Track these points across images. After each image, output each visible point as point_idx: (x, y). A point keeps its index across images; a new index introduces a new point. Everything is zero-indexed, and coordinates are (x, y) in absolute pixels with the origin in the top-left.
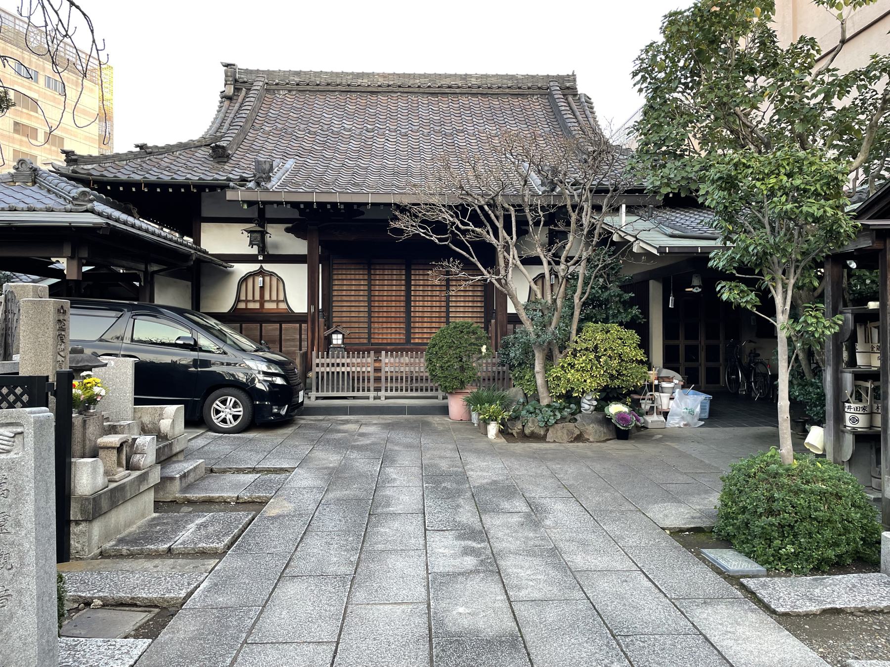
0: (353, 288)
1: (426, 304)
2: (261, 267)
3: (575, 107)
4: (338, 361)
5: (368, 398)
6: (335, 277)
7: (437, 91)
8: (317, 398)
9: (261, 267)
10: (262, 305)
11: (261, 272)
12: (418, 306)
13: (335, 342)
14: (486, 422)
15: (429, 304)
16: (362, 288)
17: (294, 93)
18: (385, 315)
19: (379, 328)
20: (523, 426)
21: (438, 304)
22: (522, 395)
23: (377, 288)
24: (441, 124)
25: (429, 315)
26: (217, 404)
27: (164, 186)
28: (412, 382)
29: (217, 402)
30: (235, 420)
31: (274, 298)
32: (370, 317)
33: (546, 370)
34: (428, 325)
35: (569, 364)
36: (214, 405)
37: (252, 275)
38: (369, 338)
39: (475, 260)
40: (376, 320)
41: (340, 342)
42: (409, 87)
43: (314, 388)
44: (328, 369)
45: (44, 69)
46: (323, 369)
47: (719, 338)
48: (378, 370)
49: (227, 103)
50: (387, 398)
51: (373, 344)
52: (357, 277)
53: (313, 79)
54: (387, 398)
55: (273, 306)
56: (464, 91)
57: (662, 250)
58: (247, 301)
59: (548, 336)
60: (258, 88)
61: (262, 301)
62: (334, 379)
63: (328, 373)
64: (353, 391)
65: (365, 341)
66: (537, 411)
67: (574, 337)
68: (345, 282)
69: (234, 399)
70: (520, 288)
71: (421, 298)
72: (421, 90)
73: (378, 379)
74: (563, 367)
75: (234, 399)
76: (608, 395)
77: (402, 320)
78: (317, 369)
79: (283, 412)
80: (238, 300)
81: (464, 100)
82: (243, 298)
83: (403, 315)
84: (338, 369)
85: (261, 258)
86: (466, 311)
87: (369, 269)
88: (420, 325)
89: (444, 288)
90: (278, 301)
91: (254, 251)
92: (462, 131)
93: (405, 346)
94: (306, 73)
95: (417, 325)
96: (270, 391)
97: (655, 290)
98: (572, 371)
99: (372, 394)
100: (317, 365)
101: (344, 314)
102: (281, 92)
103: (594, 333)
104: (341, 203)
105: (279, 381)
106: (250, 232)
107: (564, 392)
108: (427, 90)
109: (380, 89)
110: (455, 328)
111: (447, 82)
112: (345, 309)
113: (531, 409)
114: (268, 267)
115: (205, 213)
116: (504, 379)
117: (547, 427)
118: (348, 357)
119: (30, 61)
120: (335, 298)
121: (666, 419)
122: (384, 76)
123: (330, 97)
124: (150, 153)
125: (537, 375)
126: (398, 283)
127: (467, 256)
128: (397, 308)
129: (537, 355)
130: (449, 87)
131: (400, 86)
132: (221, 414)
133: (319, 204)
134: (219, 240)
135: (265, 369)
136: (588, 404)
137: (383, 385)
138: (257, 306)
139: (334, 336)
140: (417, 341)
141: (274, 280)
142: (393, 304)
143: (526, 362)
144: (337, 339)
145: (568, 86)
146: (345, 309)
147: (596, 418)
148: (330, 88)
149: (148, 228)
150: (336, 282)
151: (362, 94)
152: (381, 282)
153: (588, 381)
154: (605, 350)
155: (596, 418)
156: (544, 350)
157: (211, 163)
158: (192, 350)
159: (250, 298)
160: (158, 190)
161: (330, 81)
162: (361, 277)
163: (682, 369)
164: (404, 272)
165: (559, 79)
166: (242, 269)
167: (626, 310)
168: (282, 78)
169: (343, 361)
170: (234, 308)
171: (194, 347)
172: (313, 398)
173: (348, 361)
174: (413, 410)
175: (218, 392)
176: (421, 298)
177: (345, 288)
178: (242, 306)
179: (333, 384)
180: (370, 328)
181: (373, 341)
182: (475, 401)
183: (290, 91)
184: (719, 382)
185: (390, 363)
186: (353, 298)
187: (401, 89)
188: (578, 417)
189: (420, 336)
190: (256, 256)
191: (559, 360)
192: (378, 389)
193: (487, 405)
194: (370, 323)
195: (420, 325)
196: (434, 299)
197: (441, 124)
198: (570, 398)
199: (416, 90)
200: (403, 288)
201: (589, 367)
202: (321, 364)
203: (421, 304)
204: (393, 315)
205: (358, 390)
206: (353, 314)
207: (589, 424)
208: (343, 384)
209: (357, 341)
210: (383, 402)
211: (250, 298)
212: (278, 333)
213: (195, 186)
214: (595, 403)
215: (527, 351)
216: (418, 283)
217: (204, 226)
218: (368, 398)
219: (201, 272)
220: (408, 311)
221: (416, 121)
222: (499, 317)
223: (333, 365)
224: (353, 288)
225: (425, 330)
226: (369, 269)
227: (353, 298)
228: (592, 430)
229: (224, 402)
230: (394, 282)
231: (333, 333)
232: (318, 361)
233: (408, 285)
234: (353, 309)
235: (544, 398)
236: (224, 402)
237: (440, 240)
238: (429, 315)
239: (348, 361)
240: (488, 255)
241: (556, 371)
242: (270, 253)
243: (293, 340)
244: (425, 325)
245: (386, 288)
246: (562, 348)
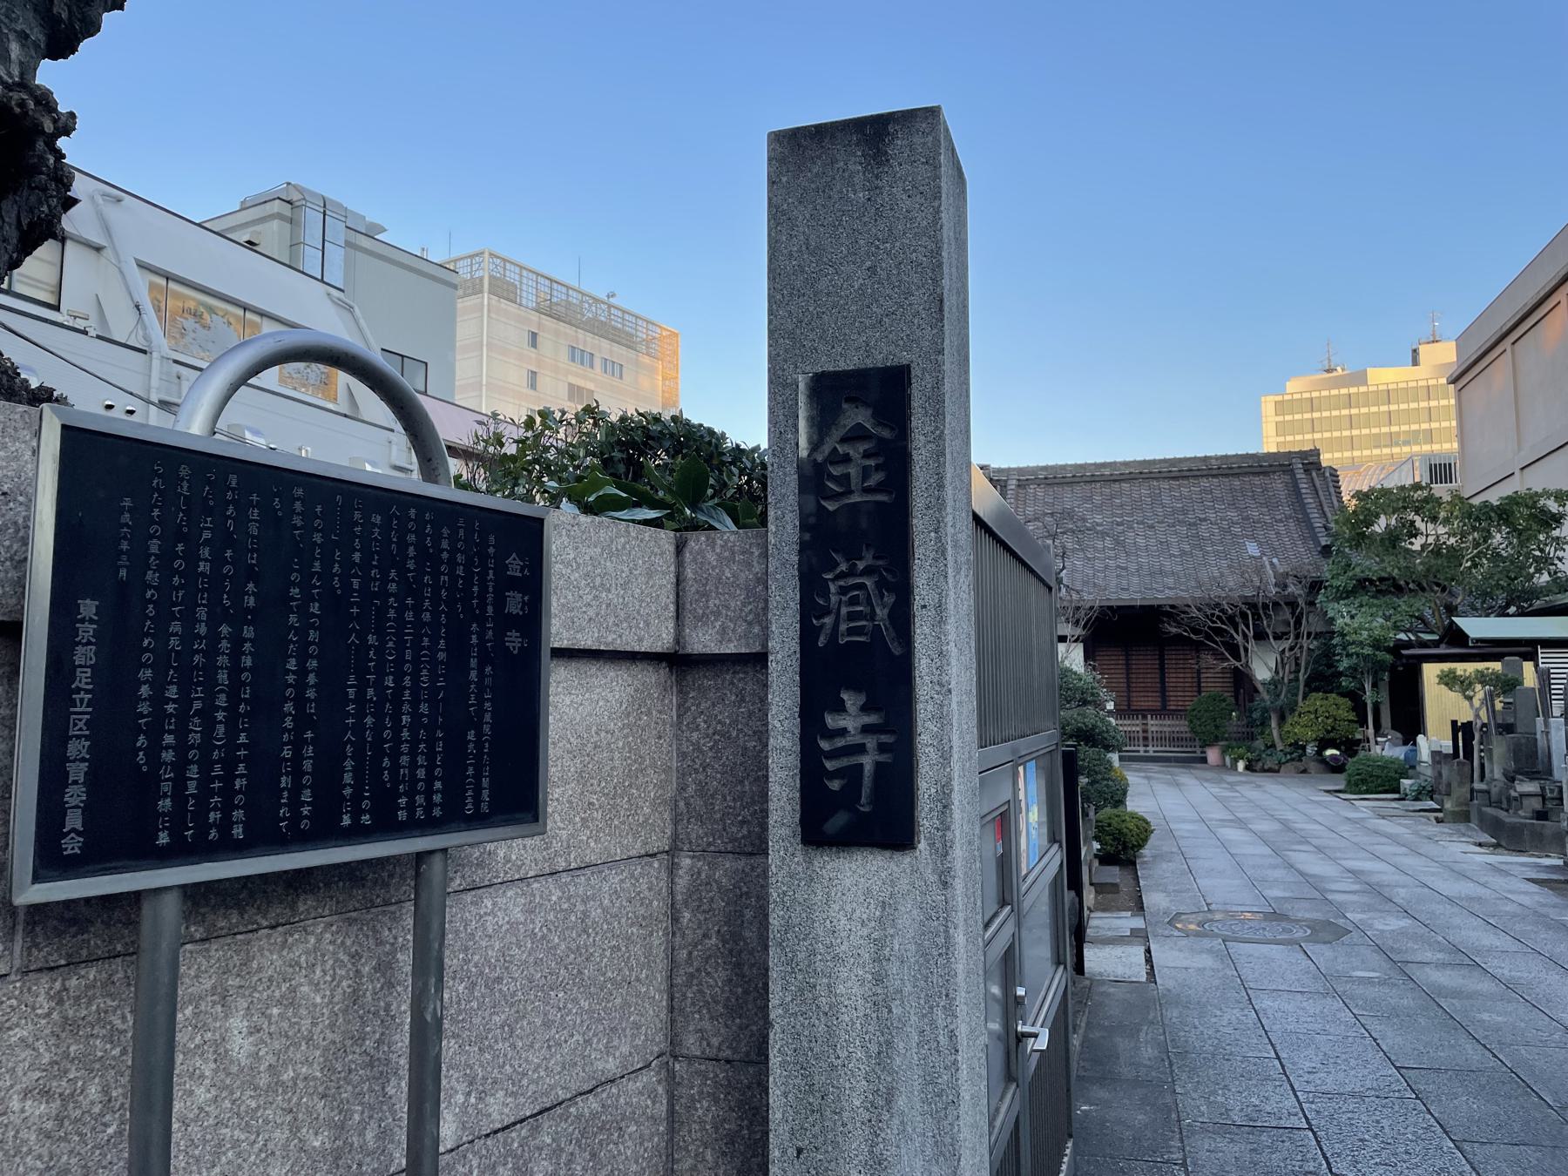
3: (1318, 483)
12: (1171, 679)
14: (1235, 761)
24: (1184, 512)
28: (1175, 740)
33: (1280, 726)
48: (1145, 731)
59: (1279, 703)
70: (1262, 668)
76: (1323, 744)
81: (1204, 483)
92: (1205, 520)
93: (1163, 711)
103: (1317, 700)
117: (1280, 764)
122: (1126, 464)
123: (1077, 488)
136: (1311, 750)
143: (1264, 723)
145: (1310, 461)
165: (1302, 455)
185: (1154, 724)
191: (1289, 720)
197: (1184, 512)
220: (1163, 682)
228: (1313, 766)
233: (1162, 668)
241: (1287, 727)
246: (1293, 710)
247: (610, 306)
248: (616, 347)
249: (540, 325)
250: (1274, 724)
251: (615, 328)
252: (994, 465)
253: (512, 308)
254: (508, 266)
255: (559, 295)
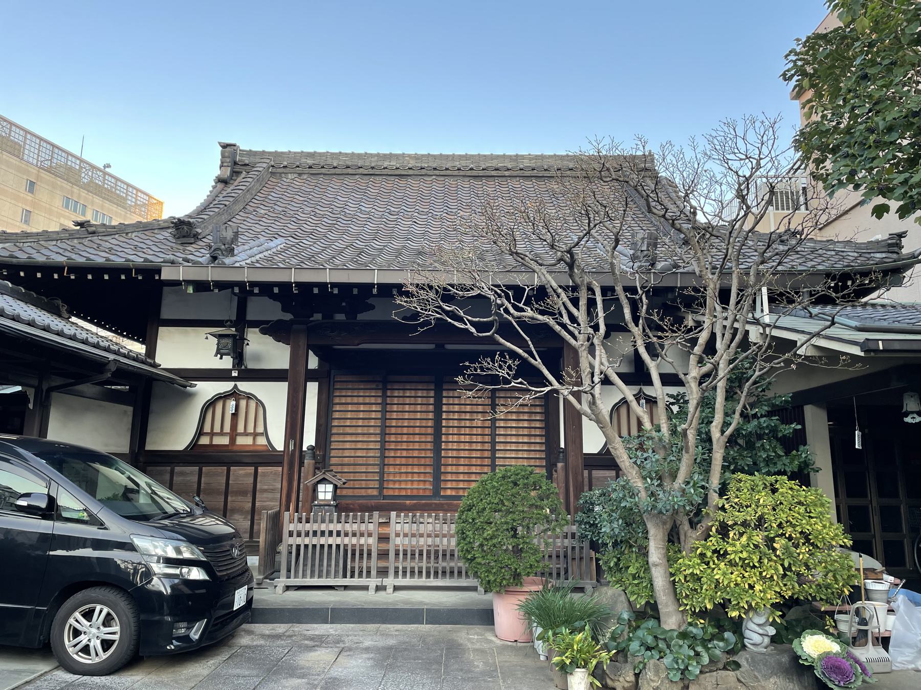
0: (361, 415)
1: (462, 438)
2: (236, 386)
4: (323, 527)
5: (366, 588)
6: (337, 400)
7: (481, 173)
8: (288, 588)
9: (236, 386)
10: (233, 440)
11: (235, 394)
12: (451, 442)
13: (321, 496)
15: (467, 439)
16: (373, 415)
17: (305, 177)
18: (404, 454)
19: (395, 473)
20: (637, 676)
21: (479, 439)
22: (626, 605)
23: (394, 416)
25: (466, 454)
26: (76, 619)
27: (98, 270)
29: (77, 615)
30: (105, 650)
31: (251, 429)
32: (383, 457)
33: (670, 561)
34: (466, 469)
35: (715, 551)
36: (71, 621)
37: (223, 397)
38: (381, 488)
39: (538, 363)
40: (391, 461)
41: (329, 496)
42: (447, 169)
43: (283, 571)
44: (307, 541)
45: (93, 203)
46: (299, 541)
47: (896, 496)
49: (220, 186)
50: (396, 588)
51: (385, 497)
52: (367, 400)
53: (329, 162)
54: (396, 588)
55: (248, 441)
56: (515, 173)
57: (872, 346)
58: (212, 434)
60: (261, 169)
61: (234, 434)
62: (311, 557)
63: (306, 546)
64: (345, 576)
65: (375, 493)
66: (662, 645)
67: (715, 499)
68: (350, 408)
69: (106, 610)
71: (455, 431)
72: (461, 173)
73: (383, 555)
74: (702, 555)
75: (106, 610)
77: (428, 462)
78: (291, 541)
79: (195, 635)
80: (200, 433)
81: (515, 183)
82: (207, 429)
83: (429, 454)
84: (323, 541)
85: (235, 374)
86: (519, 450)
87: (384, 390)
88: (454, 469)
89: (488, 409)
90: (255, 435)
91: (227, 363)
94: (321, 155)
95: (449, 469)
96: (172, 596)
97: (816, 422)
98: (722, 565)
99: (373, 582)
100: (291, 534)
101: (347, 453)
102: (290, 176)
104: (334, 285)
105: (196, 574)
106: (220, 337)
107: (709, 606)
108: (469, 173)
109: (411, 172)
110: (504, 477)
111: (494, 164)
112: (348, 446)
113: (650, 640)
114: (245, 386)
115: (165, 314)
116: (581, 558)
118: (339, 522)
119: (79, 195)
120: (334, 431)
121: (887, 649)
122: (417, 157)
123: (348, 181)
124: (94, 233)
125: (653, 570)
126: (424, 408)
127: (526, 355)
128: (423, 445)
129: (652, 531)
130: (497, 170)
131: (435, 169)
132: (82, 637)
133: (299, 285)
134: (182, 349)
135: (172, 554)
136: (758, 632)
137: (391, 563)
138: (225, 441)
139: (321, 487)
140: (449, 492)
141: (253, 404)
142: (417, 438)
143: (631, 541)
144: (325, 493)
146: (348, 446)
147: (780, 663)
148: (349, 171)
149: (85, 333)
150: (338, 408)
151: (389, 178)
152: (400, 408)
153: (758, 587)
154: (780, 526)
155: (780, 663)
156: (664, 523)
157: (172, 243)
158: (45, 517)
159: (217, 429)
160: (90, 277)
161: (349, 163)
162: (373, 400)
163: (878, 546)
164: (432, 394)
166: (207, 390)
167: (787, 453)
168: (292, 161)
169: (332, 527)
170: (194, 444)
171: (51, 510)
172: (280, 589)
173: (339, 527)
174: (436, 616)
175: (79, 596)
176: (455, 431)
177: (349, 415)
178: (205, 441)
179: (313, 565)
180: (382, 473)
181: (386, 492)
182: (545, 616)
183: (300, 174)
184: (904, 564)
185: (402, 529)
186: (359, 430)
187: (437, 172)
188: (741, 658)
189: (454, 485)
190: (229, 371)
191: (691, 538)
192: (383, 572)
193: (565, 631)
194: (383, 465)
195: (454, 469)
196: (475, 431)
198: (722, 620)
199: (456, 173)
200: (431, 416)
201: (756, 559)
202: (296, 531)
203: (456, 438)
204: (416, 454)
205: (352, 576)
206: (359, 453)
207: (767, 677)
208: (329, 565)
209: (363, 492)
210: (389, 598)
211: (217, 429)
212: (251, 480)
213: (139, 270)
214: (772, 631)
215: (632, 520)
216: (451, 408)
217: (162, 331)
218: (366, 588)
219: (145, 394)
220: (437, 449)
221: (453, 204)
222: (571, 460)
223: (315, 533)
224: (361, 415)
225: (461, 477)
226: (384, 390)
227: (359, 430)
229: (88, 615)
230: (419, 408)
231: (320, 482)
232: (292, 527)
233: (438, 412)
234: (359, 446)
235: (668, 615)
236: (88, 615)
237: (480, 327)
238: (466, 454)
239: (339, 527)
240: (557, 354)
241: (690, 564)
242: (249, 367)
243: (272, 491)
244: (461, 469)
245: (407, 416)
247: (105, 174)
248: (107, 204)
249: (38, 177)
250: (656, 553)
251: (118, 196)
252: (244, 146)
253: (14, 160)
254: (14, 128)
255: (59, 159)
